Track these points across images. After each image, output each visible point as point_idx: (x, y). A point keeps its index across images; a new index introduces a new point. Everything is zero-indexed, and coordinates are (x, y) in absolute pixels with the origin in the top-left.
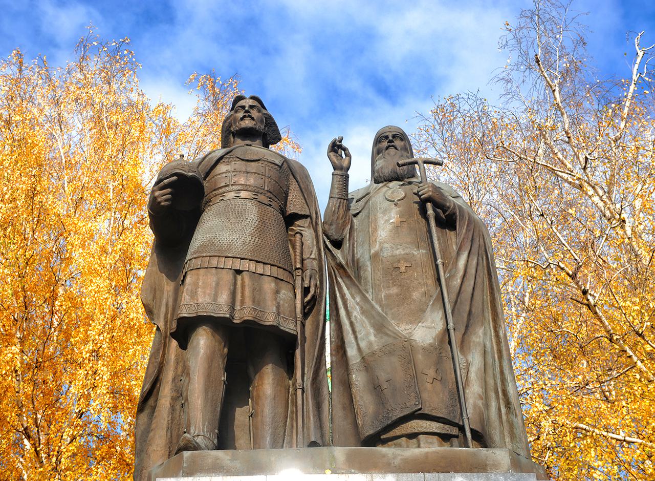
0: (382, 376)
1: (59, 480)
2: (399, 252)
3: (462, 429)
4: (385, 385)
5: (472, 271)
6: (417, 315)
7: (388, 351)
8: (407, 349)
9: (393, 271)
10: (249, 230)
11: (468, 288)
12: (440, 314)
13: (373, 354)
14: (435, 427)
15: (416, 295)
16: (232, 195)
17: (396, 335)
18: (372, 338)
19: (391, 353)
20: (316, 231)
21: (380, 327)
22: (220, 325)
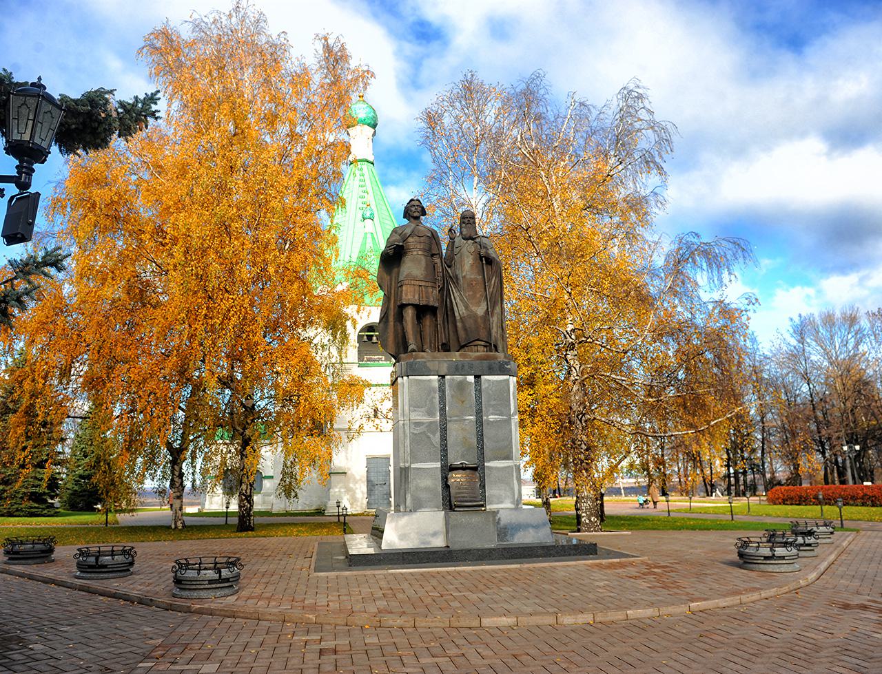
0: (468, 326)
1: (881, 563)
2: (472, 277)
3: (491, 344)
4: (468, 329)
5: (496, 284)
6: (478, 304)
7: (469, 317)
8: (474, 316)
9: (470, 285)
10: (423, 269)
11: (495, 292)
12: (486, 303)
13: (464, 317)
14: (483, 343)
15: (478, 296)
16: (415, 253)
17: (472, 311)
18: (464, 311)
19: (470, 318)
20: (441, 260)
21: (467, 307)
22: (416, 306)
